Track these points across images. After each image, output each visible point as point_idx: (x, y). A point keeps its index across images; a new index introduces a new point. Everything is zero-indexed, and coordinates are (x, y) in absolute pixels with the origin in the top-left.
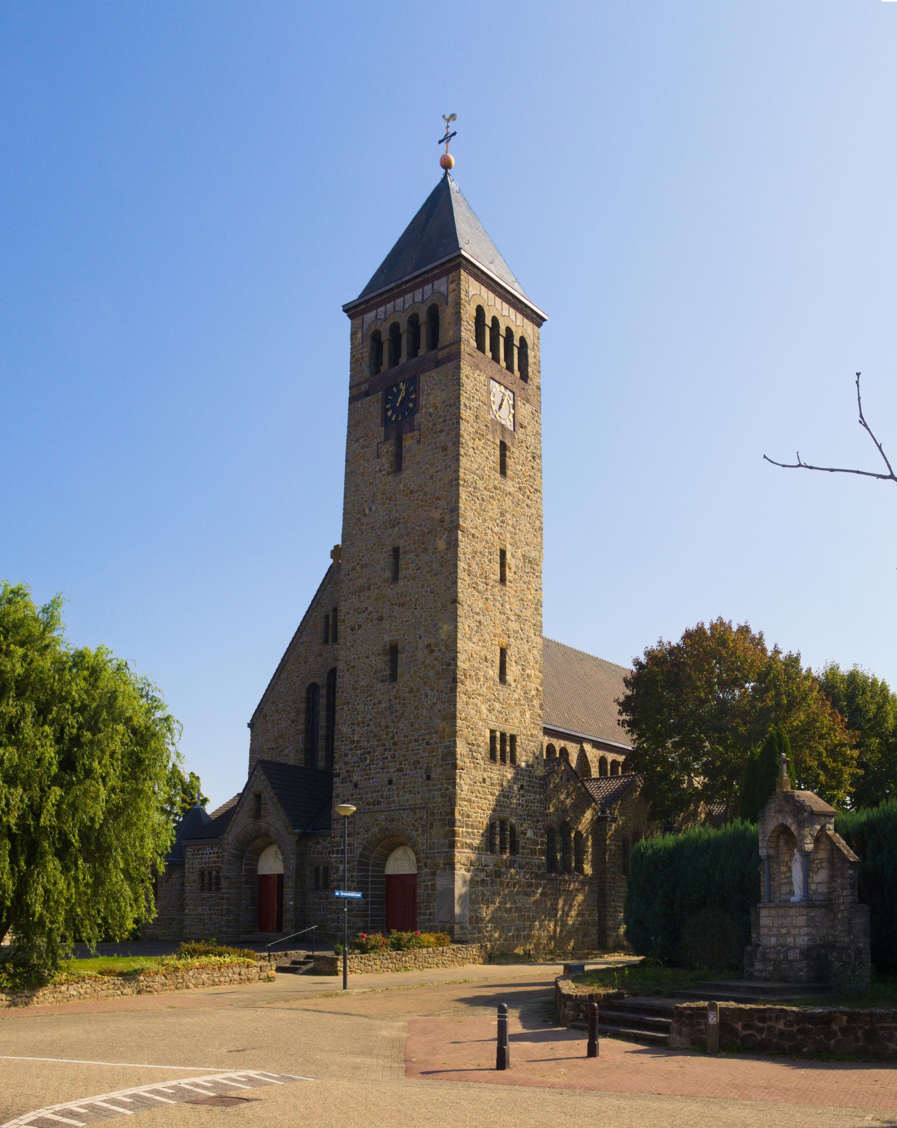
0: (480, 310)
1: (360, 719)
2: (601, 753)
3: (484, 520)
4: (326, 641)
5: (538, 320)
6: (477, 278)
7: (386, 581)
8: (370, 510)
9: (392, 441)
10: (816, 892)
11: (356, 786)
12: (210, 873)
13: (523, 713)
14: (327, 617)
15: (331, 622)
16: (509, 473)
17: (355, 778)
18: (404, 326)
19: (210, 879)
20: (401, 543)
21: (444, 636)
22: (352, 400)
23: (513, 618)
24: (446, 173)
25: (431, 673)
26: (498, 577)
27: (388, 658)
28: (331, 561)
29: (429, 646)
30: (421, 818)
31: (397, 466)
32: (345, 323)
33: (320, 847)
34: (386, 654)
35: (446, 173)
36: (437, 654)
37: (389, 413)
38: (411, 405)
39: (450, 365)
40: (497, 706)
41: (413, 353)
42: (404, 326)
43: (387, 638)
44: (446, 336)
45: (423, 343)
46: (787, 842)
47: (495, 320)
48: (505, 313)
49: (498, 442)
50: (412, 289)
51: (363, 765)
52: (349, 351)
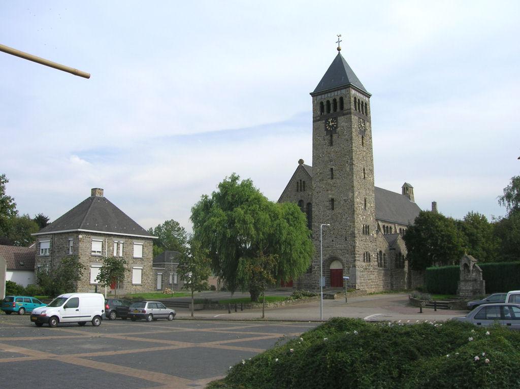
0: (355, 98)
1: (321, 221)
4: (298, 191)
5: (369, 96)
6: (354, 89)
7: (329, 178)
9: (329, 136)
13: (370, 218)
14: (298, 183)
15: (299, 185)
18: (331, 102)
20: (333, 167)
22: (314, 122)
25: (346, 208)
29: (345, 200)
31: (331, 144)
34: (329, 201)
36: (347, 202)
37: (327, 127)
39: (348, 116)
40: (364, 217)
41: (335, 109)
42: (331, 102)
43: (330, 196)
44: (346, 107)
47: (362, 102)
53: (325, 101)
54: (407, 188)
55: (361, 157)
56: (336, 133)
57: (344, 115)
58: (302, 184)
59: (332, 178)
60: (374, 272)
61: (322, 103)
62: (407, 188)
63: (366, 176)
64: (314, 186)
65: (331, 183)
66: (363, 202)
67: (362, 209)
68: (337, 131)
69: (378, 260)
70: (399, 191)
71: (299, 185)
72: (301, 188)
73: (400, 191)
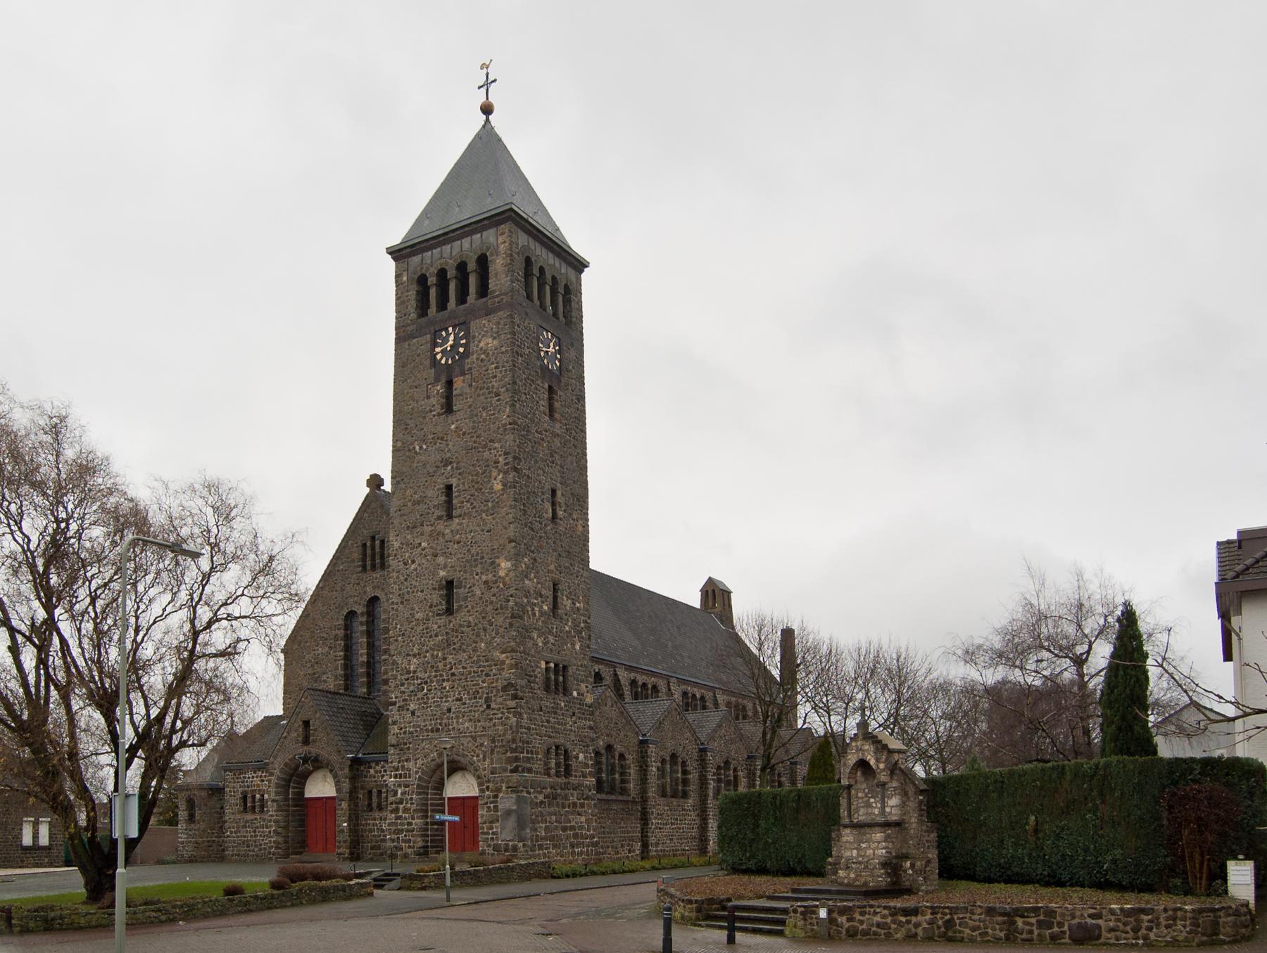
1: (416, 651)
2: (632, 675)
3: (536, 462)
4: (364, 567)
7: (440, 518)
8: (421, 448)
10: (890, 813)
11: (413, 713)
12: (254, 797)
13: (573, 645)
14: (364, 545)
15: (369, 552)
16: (557, 416)
17: (412, 707)
19: (254, 801)
20: (454, 482)
21: (502, 573)
22: (399, 340)
23: (564, 554)
24: (487, 119)
25: (490, 608)
26: (550, 515)
27: (444, 592)
28: (368, 490)
29: (486, 582)
30: (482, 745)
32: (390, 265)
33: (372, 771)
34: (440, 589)
35: (487, 119)
36: (495, 590)
38: (461, 350)
40: (551, 639)
41: (462, 299)
45: (472, 289)
46: (864, 774)
47: (542, 270)
48: (551, 261)
49: (546, 386)
50: (460, 237)
51: (420, 695)
52: (394, 293)
53: (434, 270)
54: (716, 595)
55: (543, 452)
56: (463, 374)
57: (488, 312)
58: (377, 550)
59: (450, 517)
60: (582, 806)
61: (422, 280)
62: (716, 595)
63: (560, 513)
64: (396, 545)
65: (447, 531)
66: (548, 593)
67: (542, 613)
68: (467, 367)
69: (600, 771)
70: (694, 599)
71: (369, 552)
72: (373, 559)
73: (695, 601)
